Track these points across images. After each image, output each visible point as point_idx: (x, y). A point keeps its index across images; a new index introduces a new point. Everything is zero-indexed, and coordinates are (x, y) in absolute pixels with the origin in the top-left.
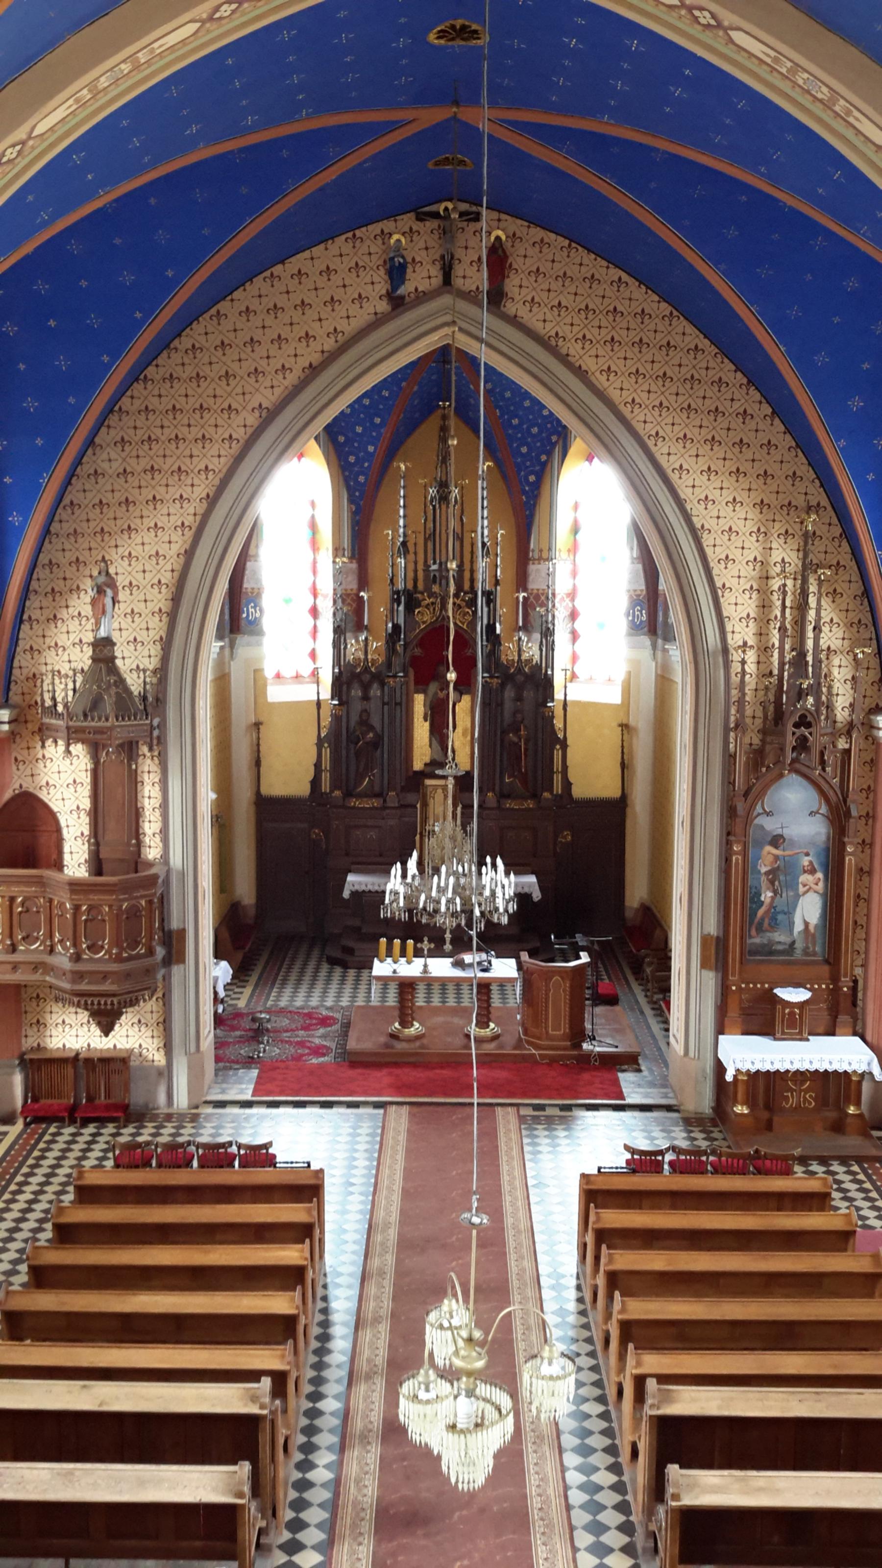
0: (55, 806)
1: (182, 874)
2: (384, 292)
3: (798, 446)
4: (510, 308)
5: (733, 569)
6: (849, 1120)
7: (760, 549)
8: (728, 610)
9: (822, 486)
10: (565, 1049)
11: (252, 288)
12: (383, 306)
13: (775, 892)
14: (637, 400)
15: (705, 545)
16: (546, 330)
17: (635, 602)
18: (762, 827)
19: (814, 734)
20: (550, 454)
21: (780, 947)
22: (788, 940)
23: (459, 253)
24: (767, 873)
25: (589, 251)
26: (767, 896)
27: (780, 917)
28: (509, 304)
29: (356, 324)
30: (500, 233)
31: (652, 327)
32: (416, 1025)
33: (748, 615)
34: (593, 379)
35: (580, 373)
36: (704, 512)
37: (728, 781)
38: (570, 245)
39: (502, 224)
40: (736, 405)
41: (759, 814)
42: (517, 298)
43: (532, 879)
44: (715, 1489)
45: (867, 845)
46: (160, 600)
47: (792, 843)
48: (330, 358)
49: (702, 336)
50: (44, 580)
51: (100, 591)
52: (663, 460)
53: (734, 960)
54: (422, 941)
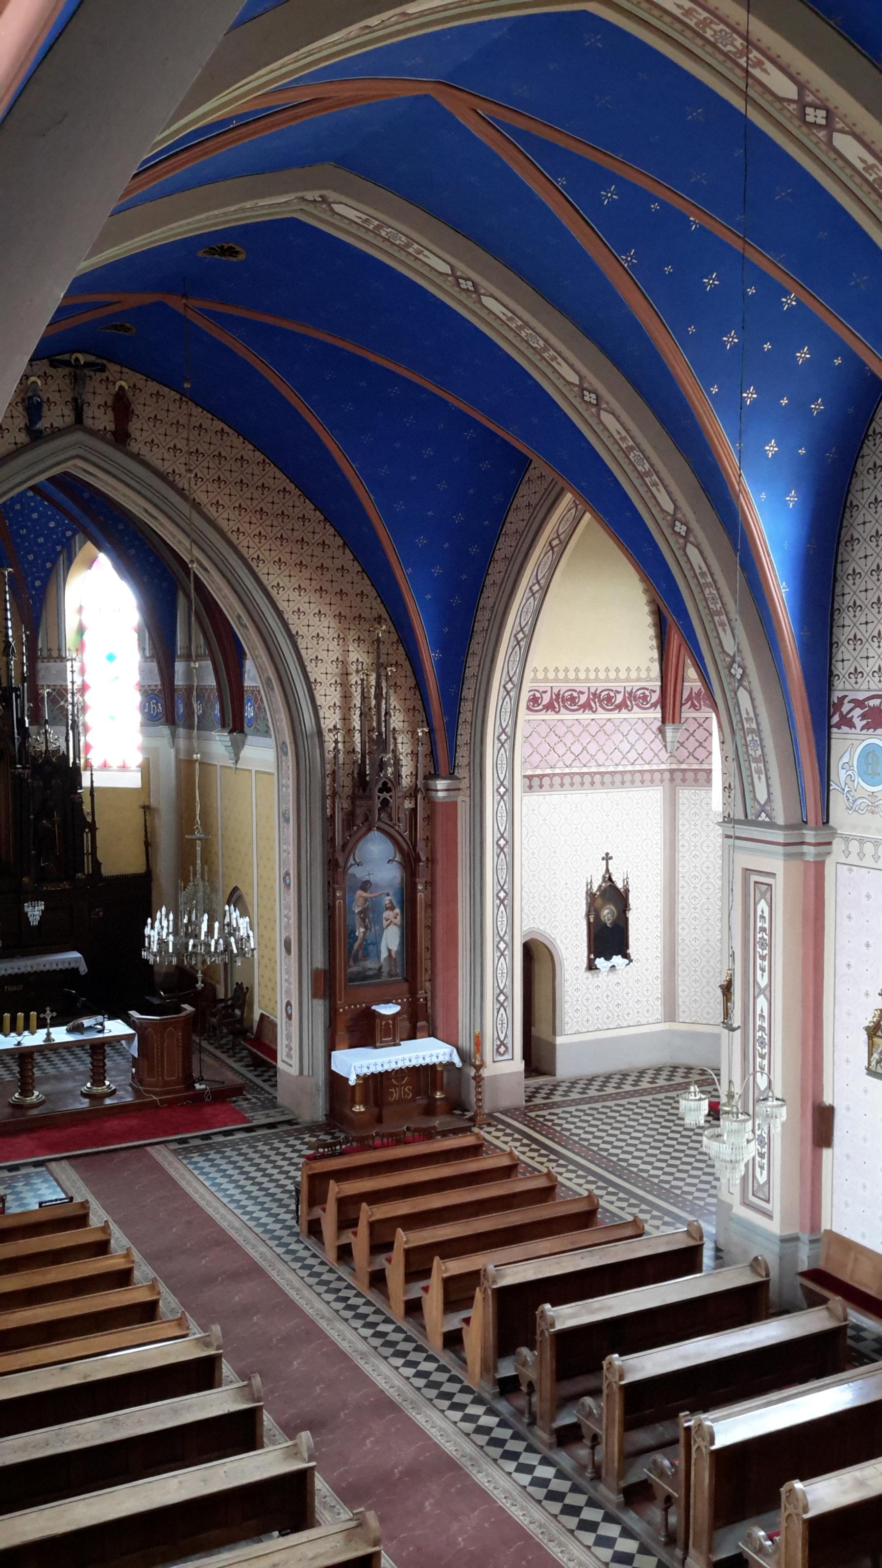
2: (22, 425)
3: (363, 571)
4: (134, 447)
5: (322, 667)
6: (438, 1103)
7: (341, 651)
8: (320, 700)
9: (382, 602)
10: (180, 1091)
12: (22, 438)
13: (366, 927)
14: (241, 529)
15: (300, 647)
16: (166, 467)
17: (148, 694)
18: (354, 876)
19: (393, 797)
20: (54, 562)
21: (371, 973)
22: (377, 966)
23: (88, 397)
24: (360, 912)
25: (197, 405)
26: (360, 931)
27: (371, 948)
28: (132, 443)
30: (123, 383)
31: (250, 471)
32: (36, 1093)
33: (335, 704)
34: (205, 510)
35: (196, 506)
36: (298, 621)
37: (329, 841)
38: (181, 399)
39: (124, 376)
40: (317, 536)
41: (352, 865)
42: (140, 439)
43: (76, 955)
44: (573, 1316)
45: (431, 884)
47: (377, 886)
49: (288, 481)
52: (264, 579)
53: (340, 987)
54: (45, 1012)
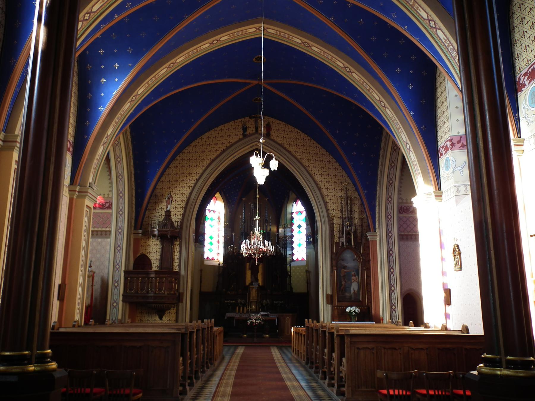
0: (151, 258)
1: (184, 277)
11: (210, 133)
12: (241, 137)
16: (281, 142)
29: (235, 140)
35: (289, 152)
46: (183, 204)
48: (228, 148)
50: (150, 207)
51: (169, 198)
